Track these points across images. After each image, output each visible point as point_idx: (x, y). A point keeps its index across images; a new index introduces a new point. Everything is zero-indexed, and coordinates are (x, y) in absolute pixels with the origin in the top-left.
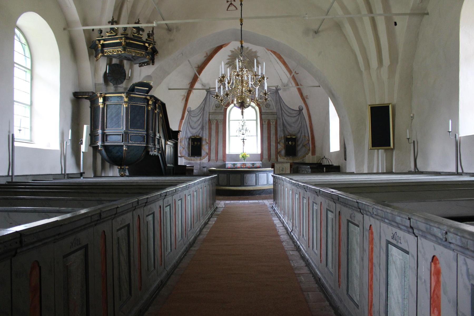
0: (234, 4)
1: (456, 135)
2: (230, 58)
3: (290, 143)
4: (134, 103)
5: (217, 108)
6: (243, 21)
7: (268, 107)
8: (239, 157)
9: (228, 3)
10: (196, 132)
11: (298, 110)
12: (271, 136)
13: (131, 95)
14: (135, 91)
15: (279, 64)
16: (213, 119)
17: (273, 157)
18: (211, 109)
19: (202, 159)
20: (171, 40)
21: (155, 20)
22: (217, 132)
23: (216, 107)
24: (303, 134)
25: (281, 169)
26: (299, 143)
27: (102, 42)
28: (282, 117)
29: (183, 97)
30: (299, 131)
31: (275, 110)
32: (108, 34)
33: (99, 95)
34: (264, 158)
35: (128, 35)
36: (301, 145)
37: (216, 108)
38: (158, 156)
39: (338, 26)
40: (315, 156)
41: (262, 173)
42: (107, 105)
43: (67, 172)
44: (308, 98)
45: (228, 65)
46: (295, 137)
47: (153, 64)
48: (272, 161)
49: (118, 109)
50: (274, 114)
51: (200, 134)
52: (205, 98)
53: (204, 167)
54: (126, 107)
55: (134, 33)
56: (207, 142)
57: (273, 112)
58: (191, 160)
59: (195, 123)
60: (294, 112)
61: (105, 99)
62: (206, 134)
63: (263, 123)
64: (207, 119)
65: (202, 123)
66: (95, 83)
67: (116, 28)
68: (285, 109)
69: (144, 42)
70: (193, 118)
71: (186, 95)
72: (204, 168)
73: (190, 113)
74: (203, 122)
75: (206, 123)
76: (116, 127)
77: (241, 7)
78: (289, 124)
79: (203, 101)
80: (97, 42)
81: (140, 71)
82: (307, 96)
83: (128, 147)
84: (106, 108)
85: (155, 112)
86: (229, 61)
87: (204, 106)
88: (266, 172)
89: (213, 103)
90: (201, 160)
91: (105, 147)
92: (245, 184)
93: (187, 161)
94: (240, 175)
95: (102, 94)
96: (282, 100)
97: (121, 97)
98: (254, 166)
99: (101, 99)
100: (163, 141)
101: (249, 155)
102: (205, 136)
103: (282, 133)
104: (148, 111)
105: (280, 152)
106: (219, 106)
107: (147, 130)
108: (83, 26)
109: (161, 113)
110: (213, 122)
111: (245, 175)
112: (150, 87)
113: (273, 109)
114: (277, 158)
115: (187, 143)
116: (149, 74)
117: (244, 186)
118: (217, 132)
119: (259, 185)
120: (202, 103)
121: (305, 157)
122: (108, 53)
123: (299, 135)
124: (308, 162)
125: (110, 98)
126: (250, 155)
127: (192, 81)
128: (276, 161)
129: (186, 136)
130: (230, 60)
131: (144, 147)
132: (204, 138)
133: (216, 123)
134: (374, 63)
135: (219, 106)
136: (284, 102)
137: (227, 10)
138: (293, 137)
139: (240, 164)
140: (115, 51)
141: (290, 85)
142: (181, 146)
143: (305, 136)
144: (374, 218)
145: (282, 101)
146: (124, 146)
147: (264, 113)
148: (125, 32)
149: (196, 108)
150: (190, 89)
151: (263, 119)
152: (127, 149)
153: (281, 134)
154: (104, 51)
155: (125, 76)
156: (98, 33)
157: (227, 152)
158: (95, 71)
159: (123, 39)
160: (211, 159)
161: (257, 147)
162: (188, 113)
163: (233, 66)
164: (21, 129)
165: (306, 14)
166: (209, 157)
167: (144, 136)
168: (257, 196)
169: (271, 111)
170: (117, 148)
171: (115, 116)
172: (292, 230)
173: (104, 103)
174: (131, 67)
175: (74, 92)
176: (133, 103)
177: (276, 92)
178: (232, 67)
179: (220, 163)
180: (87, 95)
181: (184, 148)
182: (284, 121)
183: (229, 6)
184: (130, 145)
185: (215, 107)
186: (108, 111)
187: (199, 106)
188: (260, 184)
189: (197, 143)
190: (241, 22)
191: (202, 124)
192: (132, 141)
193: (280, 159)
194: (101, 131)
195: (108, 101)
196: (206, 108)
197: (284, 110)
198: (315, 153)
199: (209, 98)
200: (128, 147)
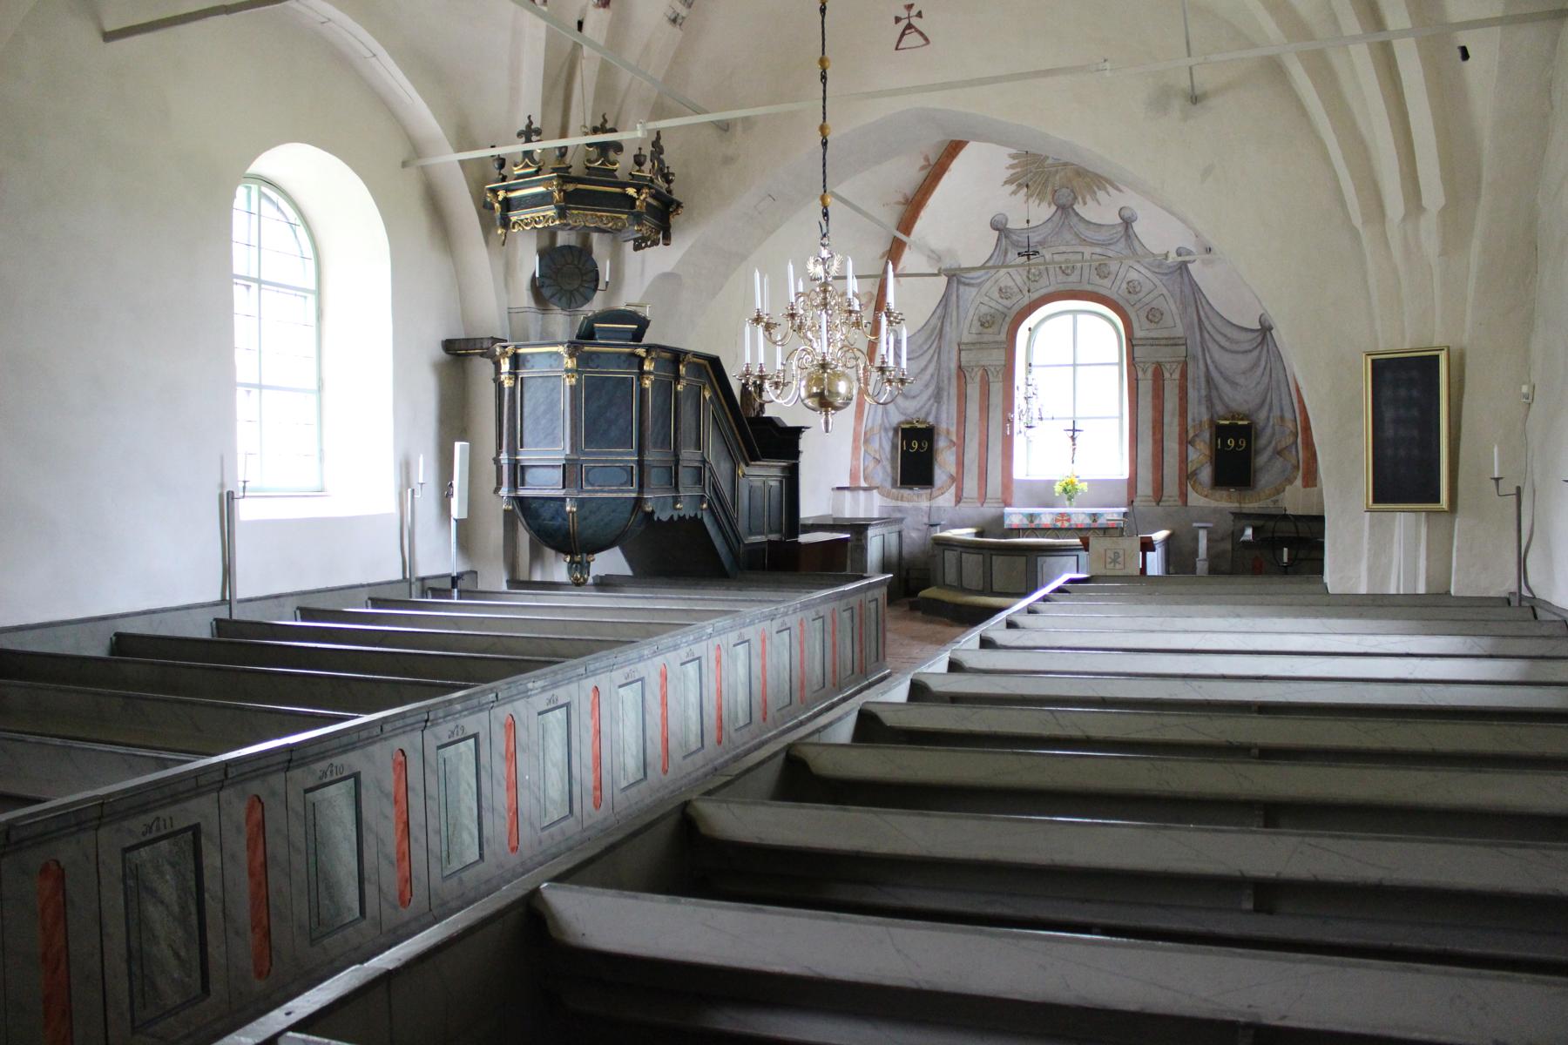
0: (917, 26)
2: (1016, 161)
3: (1231, 442)
6: (827, 131)
8: (1054, 492)
11: (1258, 330)
12: (1166, 420)
13: (586, 348)
14: (597, 336)
16: (972, 364)
17: (1171, 488)
18: (965, 332)
19: (934, 494)
20: (728, 160)
22: (985, 409)
23: (982, 325)
24: (1276, 412)
25: (1110, 558)
26: (1262, 442)
27: (501, 194)
28: (1204, 355)
30: (1263, 402)
31: (1179, 331)
35: (570, 170)
36: (1270, 450)
37: (980, 328)
38: (697, 522)
39: (1275, 69)
42: (522, 378)
43: (422, 571)
45: (1013, 187)
46: (1246, 423)
48: (1167, 504)
49: (553, 390)
50: (1176, 345)
51: (928, 414)
54: (571, 386)
55: (589, 161)
56: (951, 441)
57: (1172, 336)
58: (902, 500)
60: (1243, 336)
61: (516, 361)
62: (948, 413)
64: (953, 366)
65: (936, 376)
66: (509, 308)
68: (1213, 326)
69: (624, 185)
71: (875, 292)
74: (938, 375)
75: (949, 379)
77: (822, 85)
78: (1226, 379)
79: (938, 307)
81: (643, 262)
83: (581, 503)
85: (676, 388)
86: (1014, 174)
87: (942, 323)
93: (889, 500)
94: (1024, 559)
96: (1204, 295)
100: (722, 468)
101: (1086, 483)
102: (946, 422)
103: (1203, 409)
104: (643, 391)
105: (1195, 473)
106: (990, 322)
107: (641, 450)
108: (459, 150)
109: (707, 386)
110: (973, 375)
111: (1039, 559)
112: (643, 324)
114: (1184, 496)
115: (890, 443)
116: (668, 269)
118: (985, 409)
121: (1284, 491)
123: (1263, 415)
126: (1091, 482)
127: (891, 247)
128: (1180, 503)
129: (886, 421)
130: (1019, 170)
131: (633, 502)
132: (943, 426)
133: (982, 378)
134: (1395, 204)
135: (990, 322)
136: (1208, 302)
137: (897, 49)
138: (1240, 423)
139: (1051, 516)
142: (869, 454)
143: (1282, 418)
145: (1203, 300)
146: (568, 500)
152: (575, 509)
153: (1198, 412)
155: (597, 280)
157: (1019, 472)
165: (1105, 61)
167: (632, 467)
169: (1165, 334)
175: (444, 339)
176: (595, 372)
177: (1180, 268)
179: (989, 510)
180: (478, 346)
181: (878, 461)
182: (1211, 368)
183: (903, 34)
185: (976, 323)
186: (526, 396)
187: (923, 324)
189: (1237, 443)
192: (592, 485)
193: (1195, 499)
196: (947, 328)
197: (1209, 328)
199: (957, 297)
200: (581, 503)
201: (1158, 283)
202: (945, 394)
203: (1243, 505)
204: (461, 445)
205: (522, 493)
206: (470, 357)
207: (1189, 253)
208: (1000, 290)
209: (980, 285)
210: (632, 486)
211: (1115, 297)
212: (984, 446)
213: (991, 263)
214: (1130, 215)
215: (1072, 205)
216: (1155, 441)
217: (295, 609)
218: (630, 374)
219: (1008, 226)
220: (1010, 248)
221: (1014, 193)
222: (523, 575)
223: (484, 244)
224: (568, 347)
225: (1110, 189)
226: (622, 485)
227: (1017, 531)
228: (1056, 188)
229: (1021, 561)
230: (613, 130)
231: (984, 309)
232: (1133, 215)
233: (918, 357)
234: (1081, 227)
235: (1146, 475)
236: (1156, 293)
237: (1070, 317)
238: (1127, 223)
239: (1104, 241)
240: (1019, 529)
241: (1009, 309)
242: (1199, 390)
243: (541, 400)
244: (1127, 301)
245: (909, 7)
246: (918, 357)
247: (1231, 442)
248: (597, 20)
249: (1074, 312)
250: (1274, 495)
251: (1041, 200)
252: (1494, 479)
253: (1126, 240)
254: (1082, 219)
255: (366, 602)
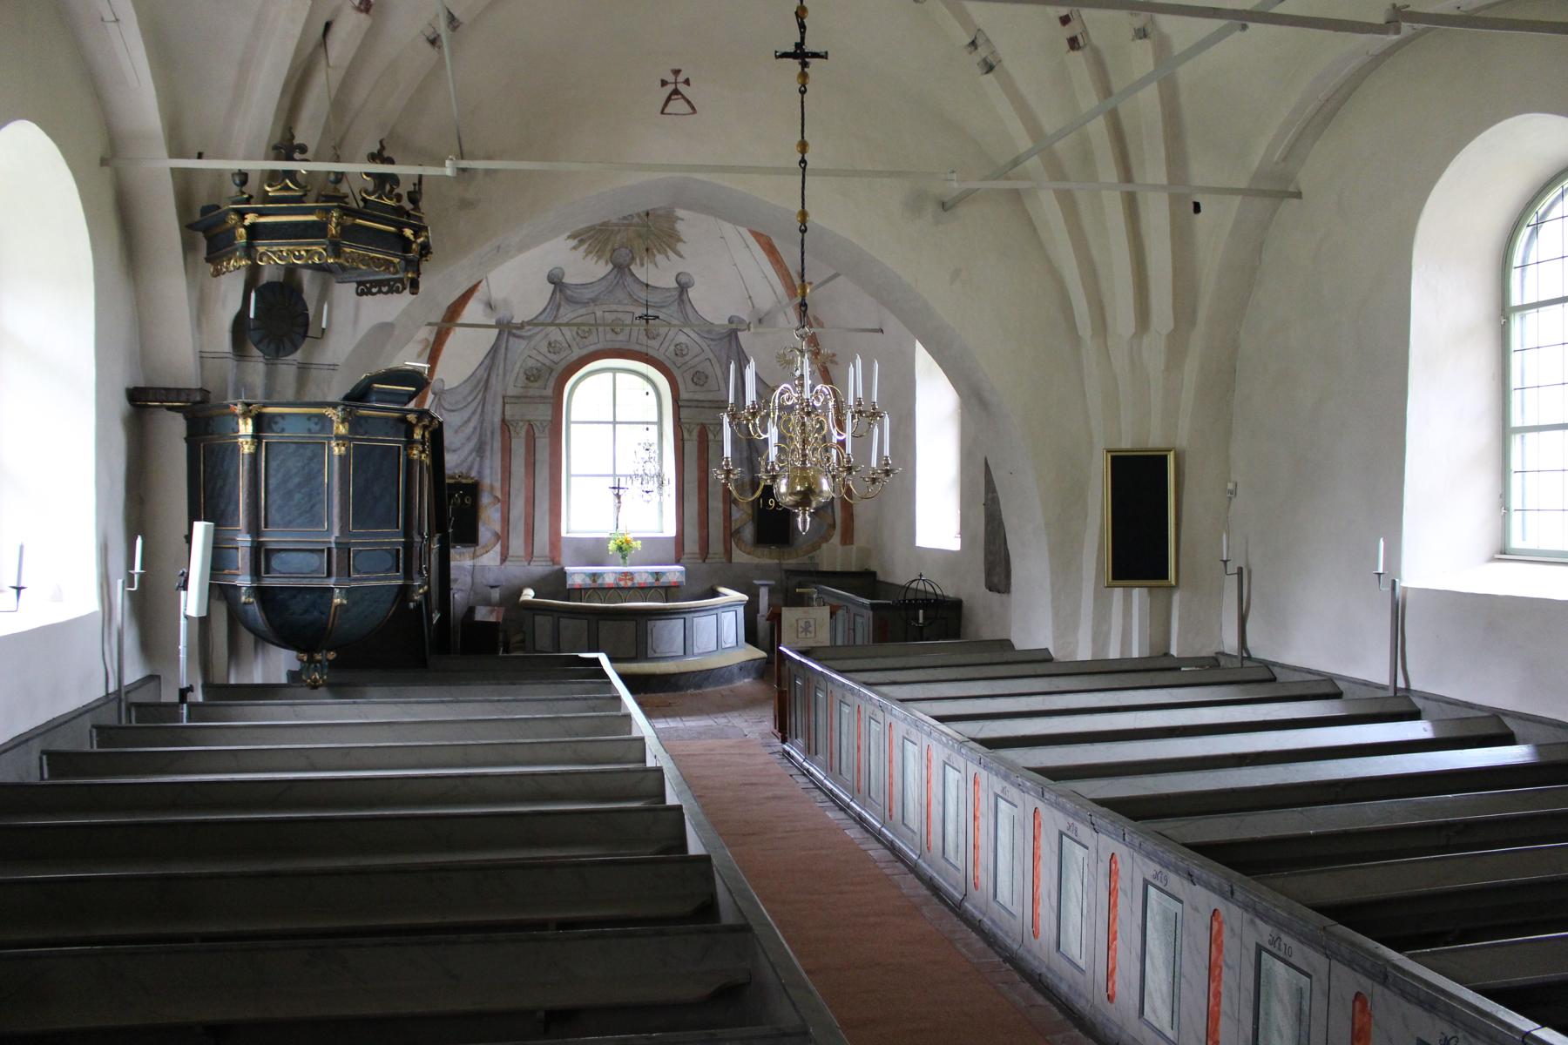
1: (1394, 582)
4: (365, 437)
5: (532, 381)
7: (702, 383)
8: (608, 550)
9: (665, 87)
10: (459, 461)
14: (374, 398)
15: (750, 250)
16: (517, 418)
17: (716, 546)
19: (478, 553)
20: (465, 204)
21: (450, 157)
22: (531, 465)
23: (528, 379)
25: (801, 627)
27: (250, 219)
29: (421, 347)
32: (274, 191)
33: (239, 409)
34: (687, 549)
35: (346, 200)
37: (526, 381)
40: (854, 547)
41: (701, 614)
44: (836, 363)
45: (574, 242)
47: (415, 291)
48: (713, 561)
49: (311, 459)
51: (470, 468)
52: (492, 349)
53: (492, 587)
55: (366, 192)
56: (496, 497)
59: (456, 432)
61: (261, 423)
62: (491, 468)
63: (683, 435)
64: (497, 419)
65: (478, 429)
66: (201, 352)
67: (304, 172)
70: (452, 414)
71: (432, 339)
72: (493, 591)
73: (439, 399)
74: (481, 428)
75: (492, 433)
76: (300, 526)
79: (485, 358)
80: (233, 217)
82: (834, 355)
84: (263, 454)
87: (489, 375)
88: (715, 612)
89: (518, 365)
90: (478, 557)
91: (261, 593)
92: (650, 654)
95: (251, 408)
97: (322, 417)
98: (662, 580)
99: (246, 424)
101: (639, 542)
102: (490, 478)
104: (409, 462)
105: (738, 531)
107: (407, 533)
110: (518, 429)
111: (649, 622)
113: (717, 388)
116: (389, 319)
117: (646, 659)
118: (531, 465)
119: (693, 655)
120: (480, 365)
121: (820, 547)
122: (270, 258)
124: (830, 569)
125: (278, 419)
128: (724, 560)
131: (396, 590)
132: (487, 481)
133: (527, 432)
137: (662, 113)
140: (299, 251)
141: (781, 320)
144: (831, 617)
146: (337, 591)
147: (687, 404)
148: (338, 186)
149: (461, 381)
150: (448, 325)
151: (683, 423)
152: (345, 602)
154: (257, 251)
156: (234, 182)
158: (202, 307)
159: (335, 215)
160: (511, 553)
161: (661, 511)
162: (434, 398)
163: (590, 245)
164: (22, 585)
165: (953, 172)
166: (502, 547)
168: (689, 691)
169: (710, 397)
170: (308, 597)
171: (299, 486)
172: (965, 895)
173: (257, 436)
174: (324, 295)
175: (132, 387)
177: (730, 335)
178: (587, 249)
179: (539, 568)
183: (669, 99)
184: (354, 585)
185: (522, 377)
186: (273, 464)
188: (696, 651)
190: (803, 222)
191: (480, 435)
192: (359, 572)
193: (739, 556)
194: (249, 539)
195: (273, 431)
196: (493, 380)
198: (852, 536)
199: (506, 348)
200: (349, 592)
201: (704, 346)
202: (488, 448)
203: (783, 562)
204: (206, 526)
205: (268, 582)
206: (151, 410)
207: (741, 321)
208: (550, 344)
209: (529, 338)
210: (398, 571)
211: (662, 358)
212: (531, 503)
213: (542, 318)
214: (688, 280)
215: (628, 266)
216: (700, 500)
217: (39, 754)
218: (395, 441)
219: (563, 281)
220: (562, 303)
221: (575, 248)
222: (218, 679)
223: (183, 271)
224: (343, 410)
225: (670, 253)
226: (388, 571)
227: (579, 592)
228: (616, 247)
229: (630, 626)
230: (391, 161)
231: (531, 363)
232: (690, 281)
233: (462, 408)
234: (635, 288)
235: (692, 533)
236: (701, 357)
237: (610, 375)
238: (683, 288)
239: (655, 303)
240: (580, 589)
241: (556, 364)
242: (741, 454)
243: (294, 471)
244: (674, 363)
245: (677, 72)
246: (462, 408)
247: (772, 502)
248: (350, 25)
249: (615, 370)
250: (811, 552)
251: (599, 258)
252: (1223, 561)
253: (679, 304)
254: (637, 280)
255: (91, 732)
